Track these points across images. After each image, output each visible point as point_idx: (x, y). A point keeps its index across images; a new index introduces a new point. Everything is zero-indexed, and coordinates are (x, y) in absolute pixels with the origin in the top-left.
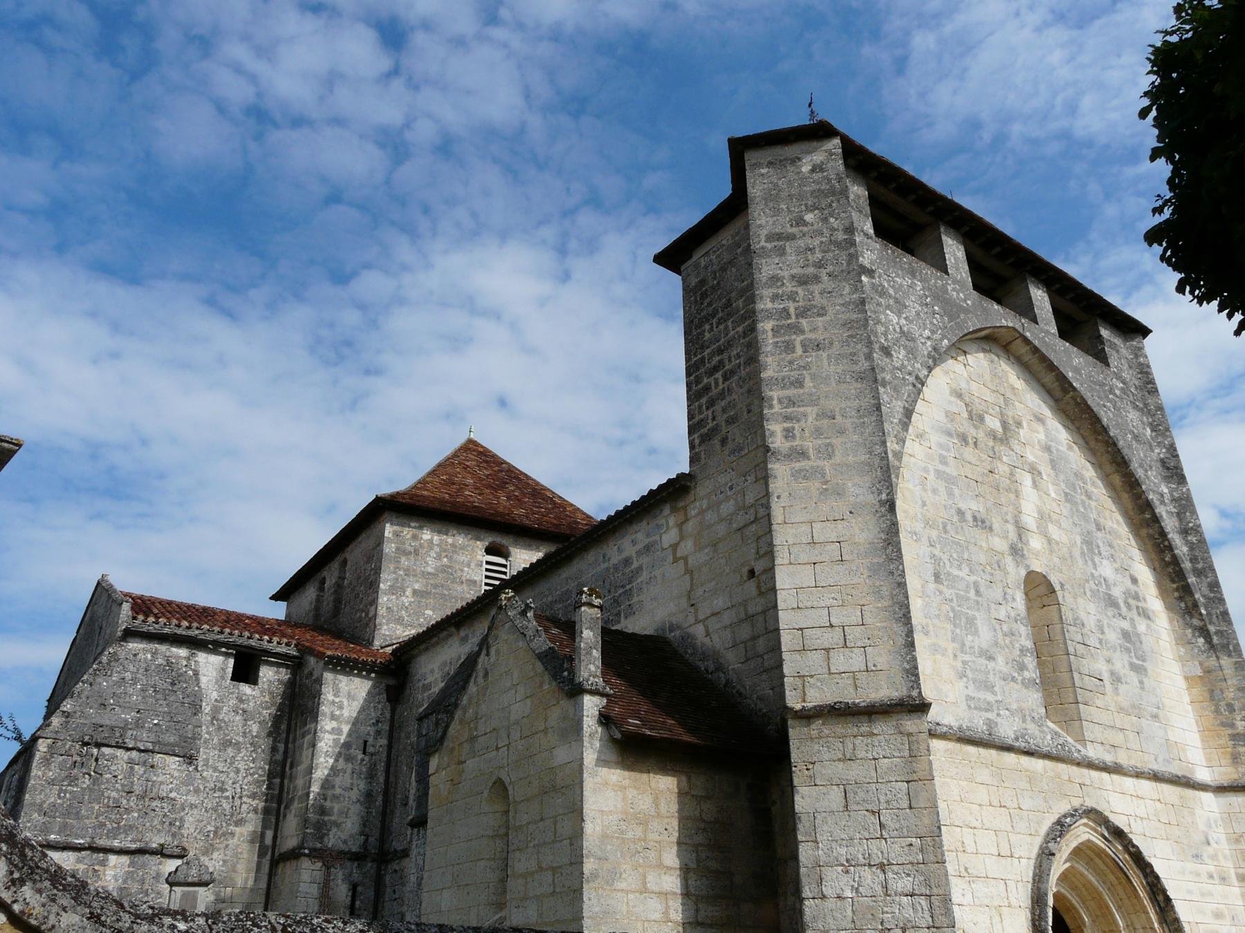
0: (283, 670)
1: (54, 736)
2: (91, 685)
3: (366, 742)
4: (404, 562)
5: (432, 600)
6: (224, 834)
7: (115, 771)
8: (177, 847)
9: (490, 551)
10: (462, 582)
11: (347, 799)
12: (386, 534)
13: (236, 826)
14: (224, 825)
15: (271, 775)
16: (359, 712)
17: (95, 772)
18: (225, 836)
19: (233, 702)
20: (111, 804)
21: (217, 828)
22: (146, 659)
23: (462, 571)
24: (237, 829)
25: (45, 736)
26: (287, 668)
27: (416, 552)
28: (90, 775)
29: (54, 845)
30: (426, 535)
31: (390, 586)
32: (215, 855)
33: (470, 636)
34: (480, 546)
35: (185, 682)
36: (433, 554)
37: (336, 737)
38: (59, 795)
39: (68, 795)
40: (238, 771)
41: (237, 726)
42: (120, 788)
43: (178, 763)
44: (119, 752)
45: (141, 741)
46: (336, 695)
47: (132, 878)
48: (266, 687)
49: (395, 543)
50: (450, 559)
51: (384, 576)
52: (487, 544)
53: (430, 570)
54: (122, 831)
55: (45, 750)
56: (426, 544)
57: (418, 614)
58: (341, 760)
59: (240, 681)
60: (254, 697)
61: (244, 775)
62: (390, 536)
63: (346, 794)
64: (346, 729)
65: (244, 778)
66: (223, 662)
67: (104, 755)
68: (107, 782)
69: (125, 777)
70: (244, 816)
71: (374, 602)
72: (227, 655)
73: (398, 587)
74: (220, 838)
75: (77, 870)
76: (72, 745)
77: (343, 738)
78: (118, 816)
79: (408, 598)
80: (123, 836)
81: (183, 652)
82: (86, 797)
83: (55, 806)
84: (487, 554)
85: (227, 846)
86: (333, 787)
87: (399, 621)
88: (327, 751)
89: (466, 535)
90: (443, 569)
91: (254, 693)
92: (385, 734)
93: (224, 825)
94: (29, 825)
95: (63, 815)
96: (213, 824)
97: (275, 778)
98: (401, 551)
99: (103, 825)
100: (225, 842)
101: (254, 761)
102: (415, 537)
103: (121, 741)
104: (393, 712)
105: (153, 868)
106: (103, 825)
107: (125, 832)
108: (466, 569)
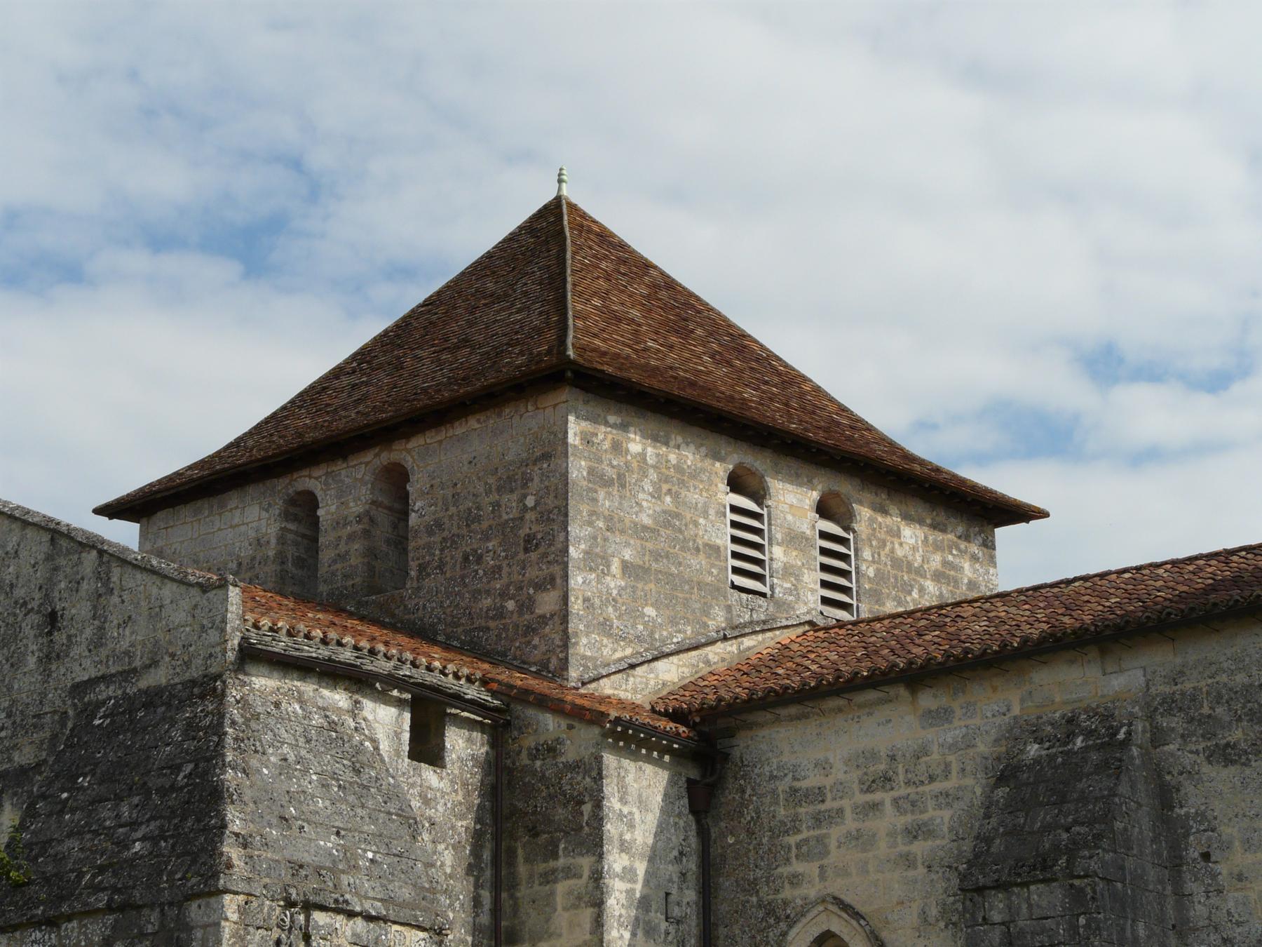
0: (477, 735)
3: (667, 894)
4: (606, 501)
5: (652, 586)
9: (736, 484)
10: (698, 549)
12: (571, 439)
16: (656, 835)
23: (696, 524)
26: (483, 732)
27: (621, 481)
30: (635, 444)
33: (959, 713)
34: (721, 470)
44: (340, 920)
46: (623, 801)
50: (676, 497)
51: (574, 529)
52: (731, 467)
53: (647, 521)
56: (635, 465)
57: (634, 614)
58: (640, 933)
60: (443, 794)
62: (577, 442)
64: (641, 868)
71: (557, 580)
72: (400, 703)
73: (597, 555)
79: (615, 582)
81: (339, 698)
84: (732, 491)
87: (605, 627)
88: (620, 916)
89: (698, 447)
90: (668, 520)
91: (442, 785)
92: (691, 877)
98: (595, 476)
104: (703, 834)
108: (701, 521)
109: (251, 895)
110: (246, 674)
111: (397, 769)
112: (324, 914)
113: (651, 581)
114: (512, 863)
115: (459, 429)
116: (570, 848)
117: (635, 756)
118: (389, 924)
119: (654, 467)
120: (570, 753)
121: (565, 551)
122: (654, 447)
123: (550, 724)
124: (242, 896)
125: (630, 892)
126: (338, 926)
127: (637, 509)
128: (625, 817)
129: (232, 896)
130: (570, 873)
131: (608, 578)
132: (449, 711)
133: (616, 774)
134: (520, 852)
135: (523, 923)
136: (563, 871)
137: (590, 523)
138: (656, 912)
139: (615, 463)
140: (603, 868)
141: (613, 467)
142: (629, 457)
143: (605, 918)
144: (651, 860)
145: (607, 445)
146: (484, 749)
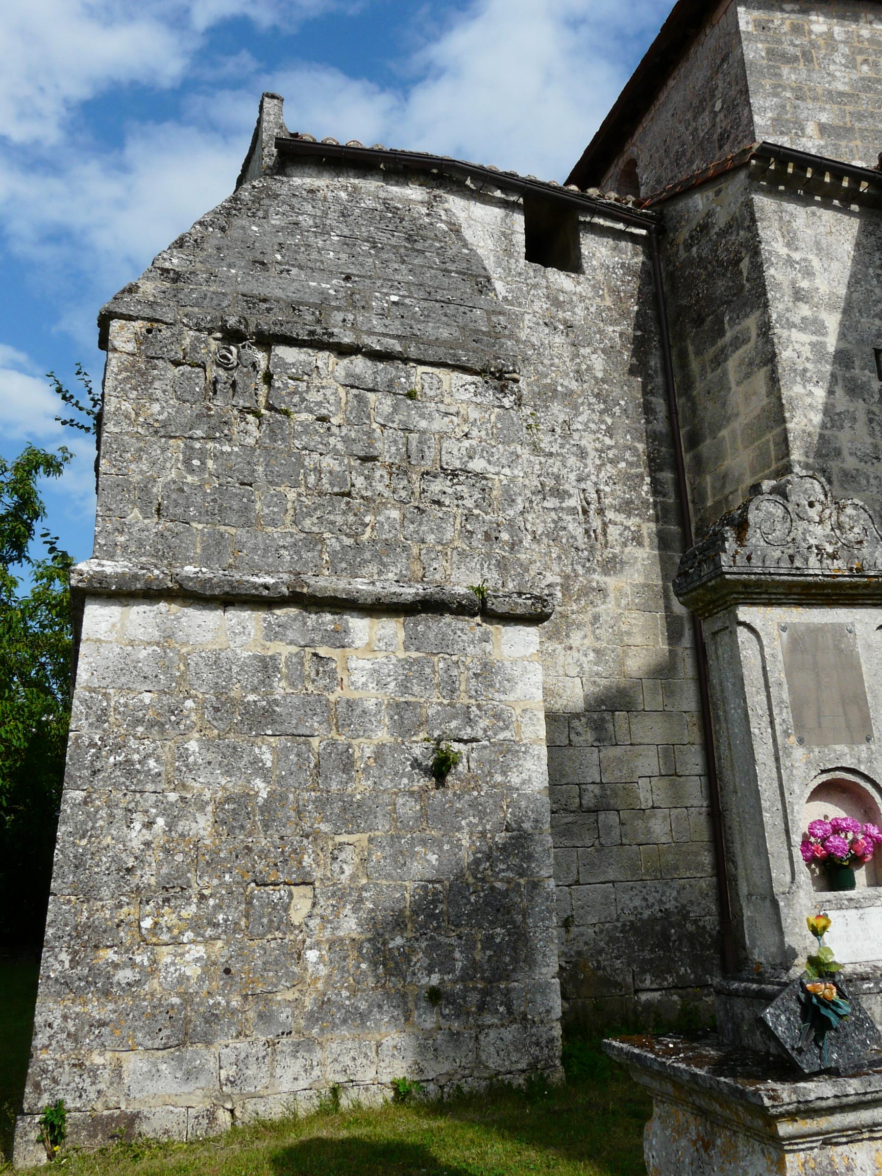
1: (148, 312)
2: (223, 229)
5: (858, 143)
6: (585, 591)
7: (319, 404)
8: (520, 594)
11: (872, 481)
12: (742, 26)
13: (606, 572)
14: (580, 571)
15: (654, 465)
17: (270, 407)
18: (586, 594)
19: (540, 305)
20: (327, 487)
21: (567, 577)
22: (337, 199)
24: (607, 579)
25: (124, 311)
27: (807, 57)
28: (257, 414)
29: (198, 588)
31: (773, 119)
32: (576, 639)
35: (436, 238)
36: (838, 58)
37: (814, 338)
38: (187, 462)
39: (210, 464)
40: (582, 454)
41: (560, 357)
42: (340, 446)
43: (472, 388)
44: (324, 359)
45: (370, 333)
46: (790, 244)
47: (422, 677)
48: (601, 278)
49: (762, 41)
51: (756, 101)
53: (841, 87)
54: (367, 555)
55: (131, 347)
56: (821, 42)
58: (839, 392)
59: (546, 263)
60: (582, 299)
61: (598, 462)
62: (751, 28)
63: (869, 469)
64: (832, 321)
65: (599, 468)
66: (503, 220)
67: (283, 364)
68: (305, 432)
69: (349, 422)
70: (617, 550)
73: (787, 121)
74: (578, 600)
75: (272, 658)
76: (197, 339)
77: (831, 343)
78: (351, 518)
80: (373, 568)
81: (414, 193)
82: (260, 469)
83: (181, 490)
85: (596, 618)
86: (838, 453)
91: (579, 289)
93: (580, 571)
94: (122, 539)
95: (207, 515)
96: (556, 568)
97: (661, 470)
98: (776, 56)
99: (314, 541)
100: (591, 611)
101: (610, 432)
102: (797, 29)
103: (319, 330)
105: (470, 650)
106: (314, 541)
107: (377, 557)
109: (157, 321)
110: (286, 175)
111: (510, 269)
112: (295, 350)
113: (856, 139)
114: (684, 365)
115: (662, 98)
116: (735, 316)
117: (806, 201)
118: (412, 364)
119: (844, 42)
120: (721, 220)
121: (751, 121)
122: (842, 26)
123: (699, 202)
124: (140, 322)
125: (818, 348)
126: (320, 364)
127: (829, 79)
128: (797, 263)
129: (124, 322)
130: (738, 342)
131: (804, 140)
132: (582, 219)
133: (777, 218)
134: (691, 348)
135: (703, 419)
136: (731, 345)
137: (776, 95)
138: (863, 369)
139: (797, 42)
140: (770, 317)
141: (796, 46)
142: (813, 37)
143: (780, 371)
144: (847, 311)
145: (786, 28)
146: (641, 258)
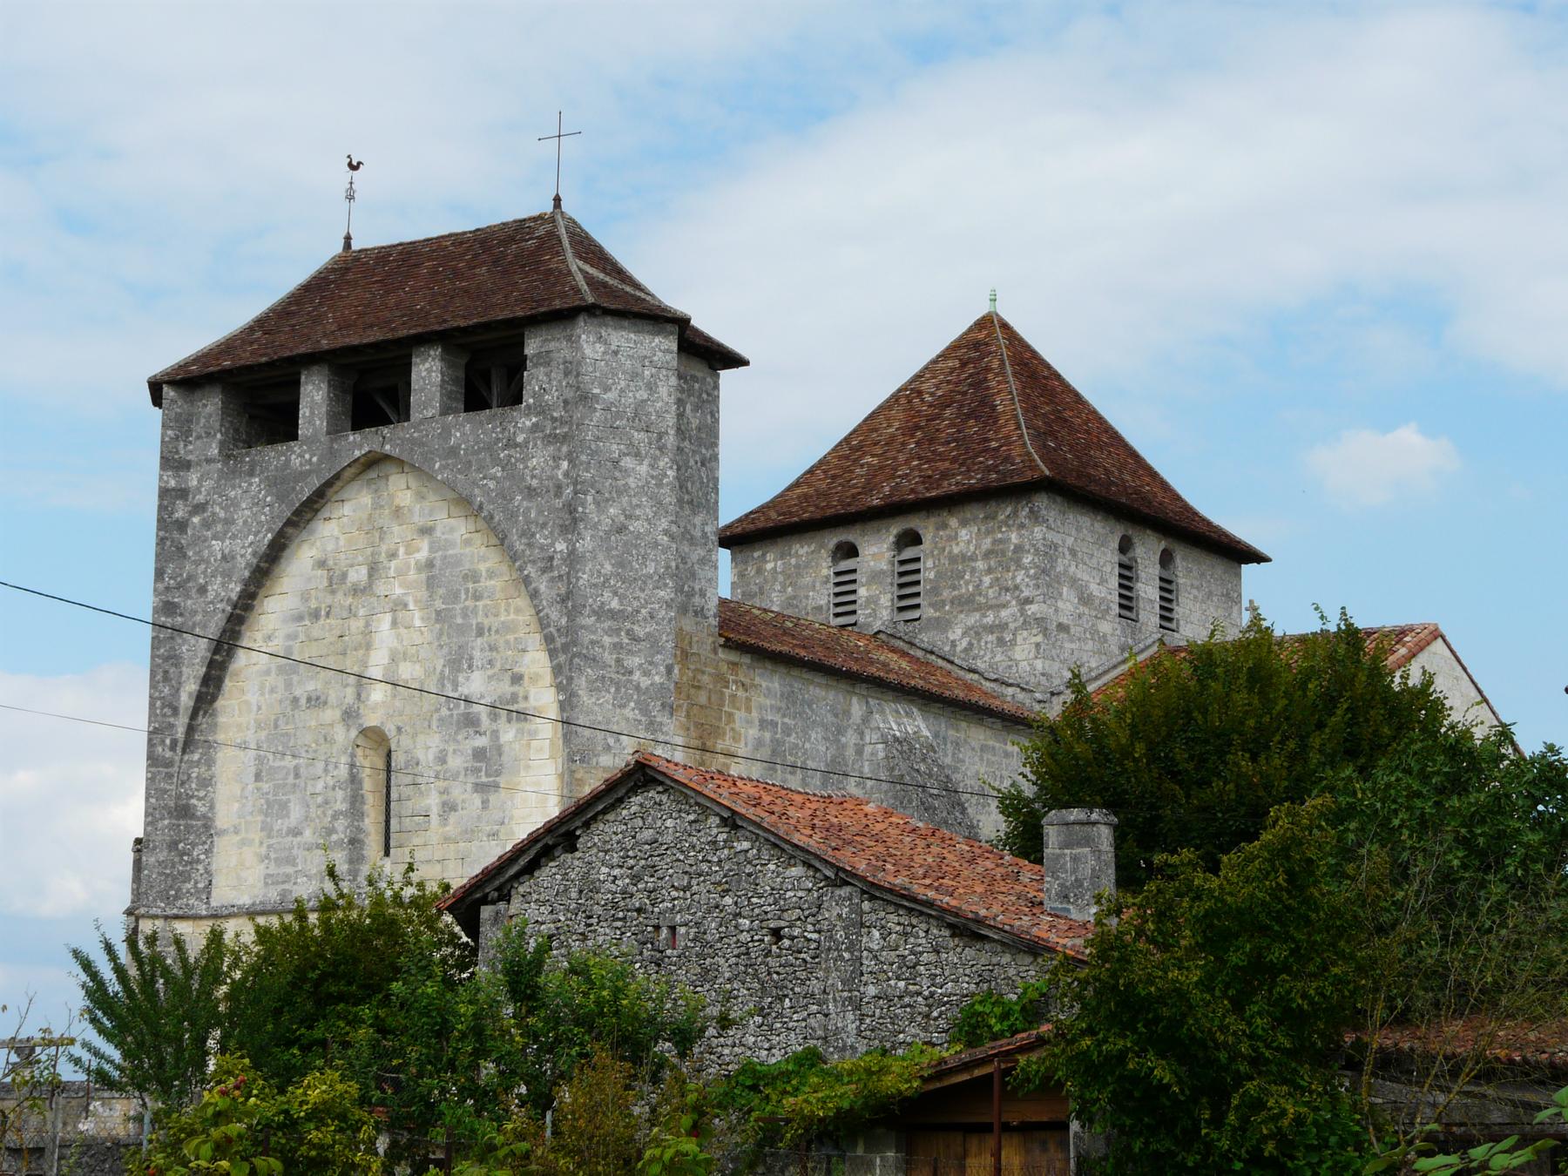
23: (807, 597)
56: (770, 577)
